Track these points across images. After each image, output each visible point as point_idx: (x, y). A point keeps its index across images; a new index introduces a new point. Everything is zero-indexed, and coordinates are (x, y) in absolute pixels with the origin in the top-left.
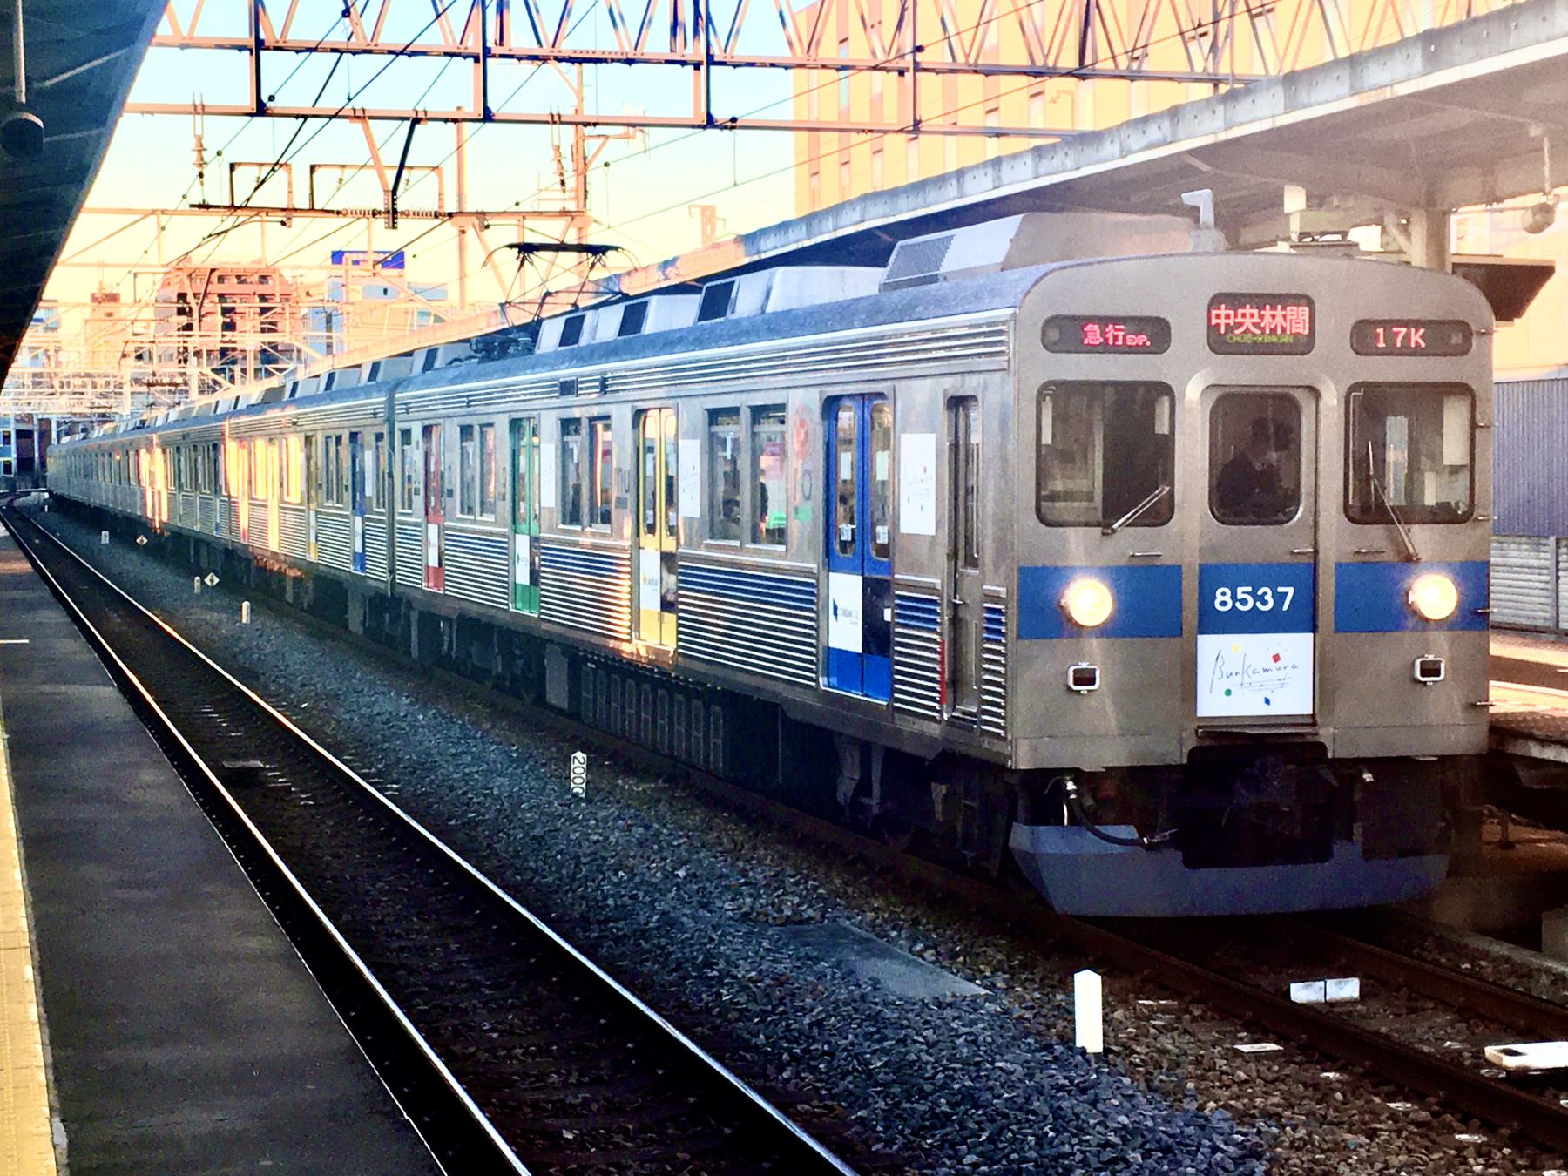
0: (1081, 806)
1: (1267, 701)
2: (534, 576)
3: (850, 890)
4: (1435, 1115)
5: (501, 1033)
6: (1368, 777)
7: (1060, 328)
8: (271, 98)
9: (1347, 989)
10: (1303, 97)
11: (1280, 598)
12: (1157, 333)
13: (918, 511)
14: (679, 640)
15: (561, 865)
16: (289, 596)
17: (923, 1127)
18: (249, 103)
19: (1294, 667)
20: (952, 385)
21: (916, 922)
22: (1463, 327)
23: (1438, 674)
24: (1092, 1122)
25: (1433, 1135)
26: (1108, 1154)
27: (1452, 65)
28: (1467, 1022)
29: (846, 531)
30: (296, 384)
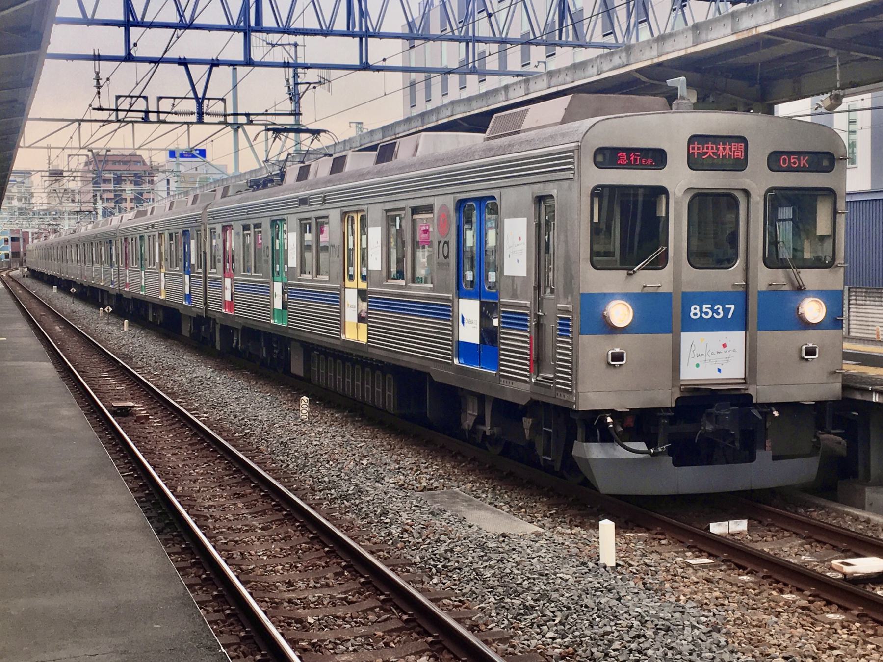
1: (719, 370)
2: (285, 305)
3: (456, 471)
4: (811, 602)
5: (268, 557)
6: (776, 414)
7: (604, 155)
8: (135, 45)
9: (740, 526)
10: (703, 37)
11: (726, 311)
12: (656, 158)
13: (516, 262)
14: (368, 338)
15: (298, 458)
16: (150, 319)
17: (519, 614)
18: (122, 53)
19: (734, 351)
20: (540, 190)
23: (815, 355)
24: (621, 612)
26: (633, 633)
28: (810, 544)
29: (469, 276)
30: (153, 208)
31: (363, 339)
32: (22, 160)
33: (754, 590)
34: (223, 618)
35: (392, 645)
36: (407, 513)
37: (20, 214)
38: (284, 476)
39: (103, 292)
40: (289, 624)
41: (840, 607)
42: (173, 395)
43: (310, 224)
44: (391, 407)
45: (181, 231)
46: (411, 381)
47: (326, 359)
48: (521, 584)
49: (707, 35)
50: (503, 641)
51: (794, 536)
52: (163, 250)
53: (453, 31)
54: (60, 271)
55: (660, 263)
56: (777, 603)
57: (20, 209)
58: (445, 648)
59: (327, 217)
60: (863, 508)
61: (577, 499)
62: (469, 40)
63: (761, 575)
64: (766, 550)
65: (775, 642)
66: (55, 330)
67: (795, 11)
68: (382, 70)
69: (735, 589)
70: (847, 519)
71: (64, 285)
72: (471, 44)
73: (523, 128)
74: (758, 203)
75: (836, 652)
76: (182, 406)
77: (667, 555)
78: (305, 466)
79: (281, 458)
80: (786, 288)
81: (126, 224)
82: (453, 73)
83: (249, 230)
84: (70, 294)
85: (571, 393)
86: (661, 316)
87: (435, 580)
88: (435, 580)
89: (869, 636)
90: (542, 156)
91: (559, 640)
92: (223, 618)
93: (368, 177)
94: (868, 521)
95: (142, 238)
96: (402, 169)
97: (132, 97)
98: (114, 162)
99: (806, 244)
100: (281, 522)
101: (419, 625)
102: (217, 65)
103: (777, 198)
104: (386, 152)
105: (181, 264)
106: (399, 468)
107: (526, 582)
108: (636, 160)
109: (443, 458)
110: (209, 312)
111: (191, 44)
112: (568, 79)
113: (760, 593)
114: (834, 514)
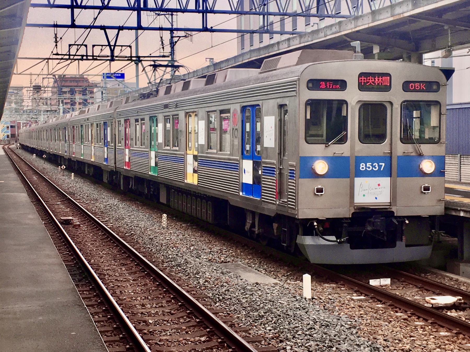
0: (319, 230)
1: (376, 198)
2: (156, 164)
3: (242, 254)
4: (409, 317)
5: (134, 293)
6: (407, 222)
9: (386, 282)
10: (377, 18)
12: (341, 85)
13: (269, 140)
14: (198, 181)
15: (157, 246)
16: (86, 173)
19: (384, 188)
20: (281, 101)
21: (260, 263)
22: (438, 84)
24: (305, 317)
25: (408, 322)
27: (421, 7)
28: (422, 291)
29: (248, 147)
30: (89, 109)
31: (196, 183)
32: (15, 81)
33: (382, 311)
34: (107, 319)
35: (189, 332)
36: (209, 272)
37: (16, 112)
38: (149, 255)
39: (61, 157)
40: (140, 323)
41: (424, 319)
42: (95, 214)
43: (169, 119)
44: (210, 220)
45: (102, 122)
46: (220, 205)
47: (182, 195)
48: (259, 305)
49: (379, 17)
50: (246, 331)
51: (415, 287)
52: (93, 133)
53: (255, 9)
54: (37, 145)
55: (343, 140)
56: (392, 317)
57: (15, 109)
58: (215, 334)
59: (178, 115)
60: (458, 274)
61: (292, 262)
62: (265, 14)
63: (388, 304)
64: (398, 293)
65: (383, 333)
66: (33, 179)
67: (422, 5)
68: (215, 31)
69: (373, 310)
70: (446, 278)
71: (40, 153)
72: (266, 16)
73: (278, 67)
74: (397, 108)
75: (412, 338)
76: (99, 220)
77: (342, 295)
78: (160, 250)
79: (149, 246)
80: (414, 154)
81: (73, 118)
82: (256, 33)
83: (138, 122)
84: (42, 158)
85: (295, 209)
86: (343, 169)
87: (217, 305)
88: (217, 305)
89: (433, 332)
90: (285, 83)
91: (273, 331)
92: (107, 319)
93: (198, 93)
94: (457, 280)
95: (82, 126)
96: (220, 88)
97: (78, 45)
98: (71, 81)
99: (427, 131)
100: (144, 277)
101: (205, 324)
102: (122, 30)
103: (408, 107)
104: (210, 79)
105: (103, 141)
106: (211, 252)
107: (262, 304)
108: (330, 86)
109: (237, 247)
110: (117, 168)
111: (107, 18)
112: (310, 39)
113: (385, 312)
114: (440, 277)
